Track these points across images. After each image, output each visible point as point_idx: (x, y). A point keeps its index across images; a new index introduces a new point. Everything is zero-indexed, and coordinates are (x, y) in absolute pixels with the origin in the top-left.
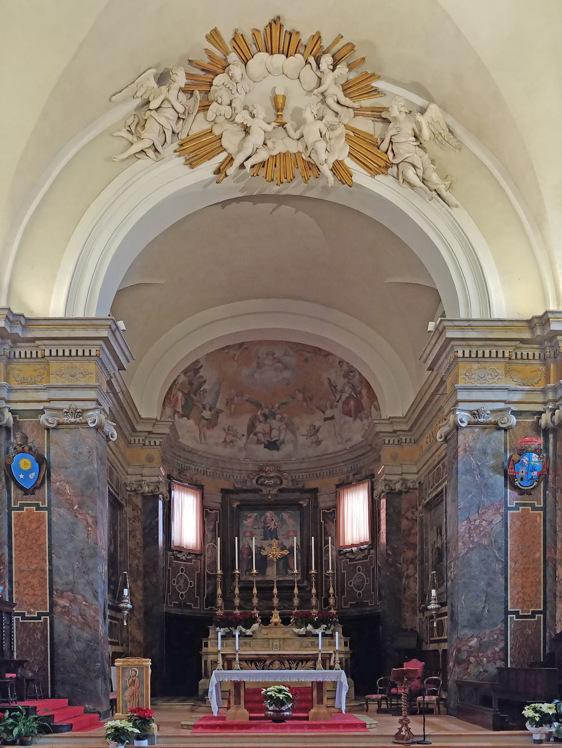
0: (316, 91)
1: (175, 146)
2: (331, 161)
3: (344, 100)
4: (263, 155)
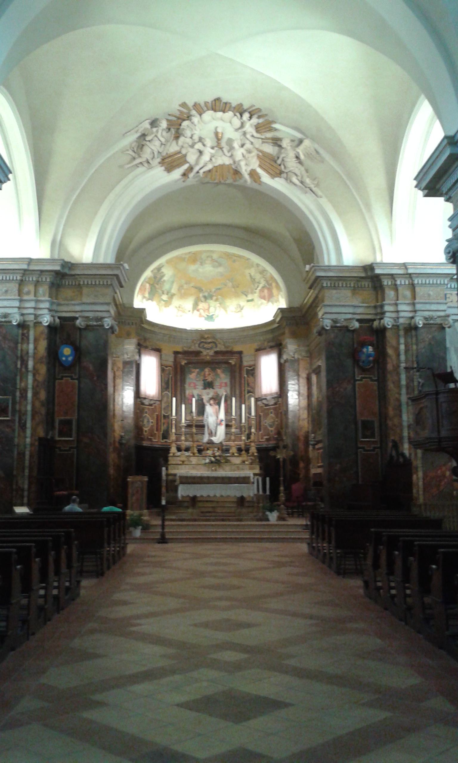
0: (240, 131)
1: (159, 160)
2: (249, 169)
3: (255, 134)
4: (210, 167)
